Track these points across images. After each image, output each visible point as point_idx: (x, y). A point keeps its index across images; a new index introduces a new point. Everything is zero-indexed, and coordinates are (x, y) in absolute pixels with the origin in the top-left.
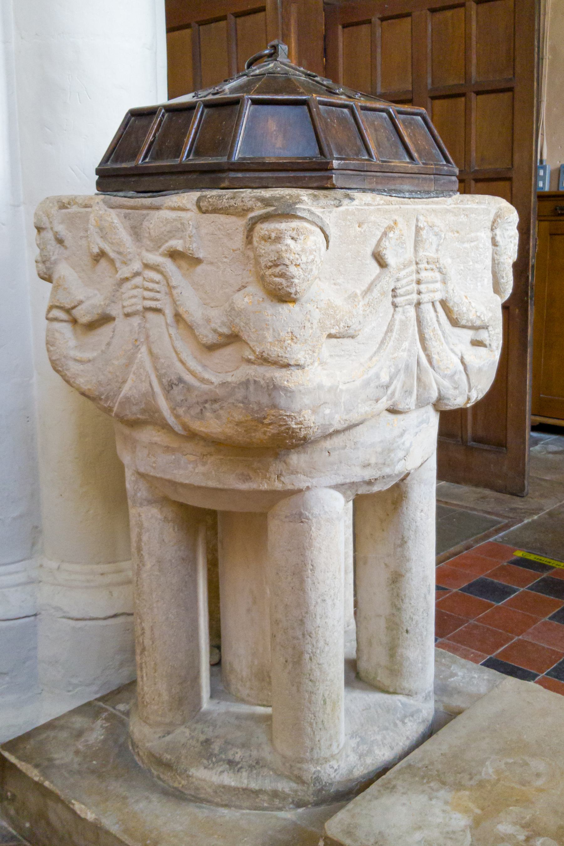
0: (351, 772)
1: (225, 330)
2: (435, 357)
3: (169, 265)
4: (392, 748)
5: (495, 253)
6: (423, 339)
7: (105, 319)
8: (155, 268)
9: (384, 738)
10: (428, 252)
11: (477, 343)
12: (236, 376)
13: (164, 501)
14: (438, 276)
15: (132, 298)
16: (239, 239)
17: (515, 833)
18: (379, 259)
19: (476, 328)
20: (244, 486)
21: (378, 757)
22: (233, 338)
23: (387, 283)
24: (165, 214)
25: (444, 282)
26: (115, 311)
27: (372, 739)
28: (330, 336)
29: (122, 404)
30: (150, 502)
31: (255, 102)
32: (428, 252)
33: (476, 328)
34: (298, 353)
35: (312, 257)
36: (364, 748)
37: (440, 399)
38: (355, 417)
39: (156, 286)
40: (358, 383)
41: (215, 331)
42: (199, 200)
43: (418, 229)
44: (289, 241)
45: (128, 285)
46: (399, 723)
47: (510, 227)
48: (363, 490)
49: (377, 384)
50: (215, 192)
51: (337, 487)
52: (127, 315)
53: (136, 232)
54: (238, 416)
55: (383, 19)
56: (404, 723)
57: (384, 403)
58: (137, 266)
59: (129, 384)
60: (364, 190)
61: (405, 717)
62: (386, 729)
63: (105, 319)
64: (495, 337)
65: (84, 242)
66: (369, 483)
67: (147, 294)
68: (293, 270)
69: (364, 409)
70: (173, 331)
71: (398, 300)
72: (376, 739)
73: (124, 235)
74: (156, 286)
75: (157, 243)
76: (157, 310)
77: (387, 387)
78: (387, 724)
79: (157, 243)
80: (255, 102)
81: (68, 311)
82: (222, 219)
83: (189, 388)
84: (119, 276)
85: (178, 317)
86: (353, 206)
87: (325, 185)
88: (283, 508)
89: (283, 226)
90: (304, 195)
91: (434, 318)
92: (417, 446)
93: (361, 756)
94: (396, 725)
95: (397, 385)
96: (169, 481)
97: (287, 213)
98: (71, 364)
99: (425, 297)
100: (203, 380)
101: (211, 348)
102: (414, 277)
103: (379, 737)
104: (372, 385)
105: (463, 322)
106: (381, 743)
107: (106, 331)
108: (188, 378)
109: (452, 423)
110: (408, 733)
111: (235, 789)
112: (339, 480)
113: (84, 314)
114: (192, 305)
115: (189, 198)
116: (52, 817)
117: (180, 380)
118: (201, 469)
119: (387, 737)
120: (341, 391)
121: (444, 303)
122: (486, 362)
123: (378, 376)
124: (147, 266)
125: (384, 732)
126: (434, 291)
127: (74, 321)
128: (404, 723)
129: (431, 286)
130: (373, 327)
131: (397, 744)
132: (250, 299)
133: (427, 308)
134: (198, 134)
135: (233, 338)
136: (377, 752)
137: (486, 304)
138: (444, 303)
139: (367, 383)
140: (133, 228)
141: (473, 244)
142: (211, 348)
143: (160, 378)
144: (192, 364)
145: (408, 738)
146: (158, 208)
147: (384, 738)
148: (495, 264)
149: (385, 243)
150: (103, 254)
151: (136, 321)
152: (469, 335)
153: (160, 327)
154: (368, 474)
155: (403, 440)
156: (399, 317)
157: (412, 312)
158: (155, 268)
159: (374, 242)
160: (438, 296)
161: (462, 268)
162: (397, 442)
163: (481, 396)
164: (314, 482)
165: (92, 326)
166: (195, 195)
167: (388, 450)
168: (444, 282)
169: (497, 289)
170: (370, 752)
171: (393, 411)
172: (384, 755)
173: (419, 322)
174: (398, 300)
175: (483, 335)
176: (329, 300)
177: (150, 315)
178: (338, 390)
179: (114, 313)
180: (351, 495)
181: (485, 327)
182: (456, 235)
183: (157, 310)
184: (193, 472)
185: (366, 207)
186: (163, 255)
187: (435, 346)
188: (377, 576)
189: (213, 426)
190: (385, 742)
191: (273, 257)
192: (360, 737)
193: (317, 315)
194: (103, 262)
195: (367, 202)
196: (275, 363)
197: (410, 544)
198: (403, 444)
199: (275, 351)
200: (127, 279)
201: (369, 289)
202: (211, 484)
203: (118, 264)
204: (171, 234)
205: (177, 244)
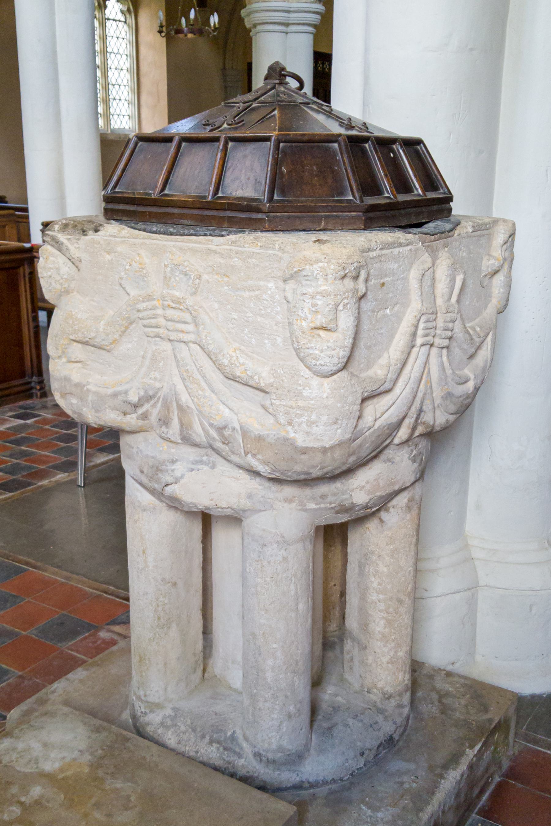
0: (148, 724)
4: (179, 743)
9: (184, 733)
17: (29, 796)
21: (166, 736)
27: (179, 724)
35: (49, 273)
36: (169, 722)
40: (110, 391)
46: (208, 738)
47: (308, 283)
49: (124, 399)
56: (211, 742)
61: (219, 742)
62: (194, 730)
72: (180, 727)
78: (199, 729)
86: (99, 236)
93: (162, 724)
94: (203, 737)
103: (183, 728)
104: (120, 398)
106: (178, 732)
110: (202, 751)
119: (187, 734)
120: (88, 390)
123: (126, 392)
125: (190, 730)
128: (211, 742)
131: (186, 746)
134: (302, 144)
136: (170, 733)
139: (115, 395)
141: (252, 293)
145: (197, 752)
147: (184, 733)
155: (173, 467)
161: (236, 317)
162: (167, 466)
170: (167, 728)
172: (169, 739)
176: (71, 311)
178: (85, 389)
182: (226, 279)
185: (112, 239)
190: (181, 734)
192: (176, 714)
195: (111, 234)
198: (173, 471)
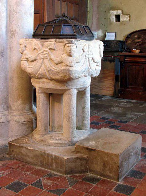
1: (60, 61)
2: (91, 67)
3: (49, 50)
5: (100, 50)
6: (89, 64)
7: (35, 60)
8: (46, 51)
10: (90, 49)
11: (97, 66)
12: (63, 68)
13: (44, 93)
14: (91, 53)
15: (41, 56)
16: (62, 47)
18: (83, 51)
19: (97, 63)
20: (60, 88)
22: (61, 62)
23: (84, 54)
24: (48, 42)
25: (93, 54)
26: (38, 59)
28: (77, 62)
29: (38, 75)
30: (41, 93)
31: (64, 25)
32: (90, 49)
33: (97, 63)
34: (72, 64)
37: (92, 75)
38: (80, 76)
39: (47, 54)
41: (58, 61)
42: (55, 40)
43: (89, 46)
44: (72, 47)
45: (41, 54)
48: (80, 90)
50: (58, 39)
51: (76, 89)
52: (40, 59)
53: (42, 45)
54: (62, 75)
55: (75, 4)
57: (84, 74)
58: (42, 51)
59: (40, 71)
60: (81, 39)
63: (35, 60)
64: (100, 64)
65: (31, 47)
66: (81, 88)
67: (44, 55)
68: (72, 51)
69: (81, 75)
70: (49, 62)
71: (86, 57)
73: (40, 46)
74: (47, 54)
75: (47, 47)
76: (47, 58)
77: (84, 71)
79: (47, 47)
80: (64, 25)
81: (27, 59)
82: (59, 43)
83: (53, 71)
84: (39, 52)
85: (50, 59)
87: (75, 38)
88: (67, 92)
89: (71, 45)
90: (73, 40)
91: (91, 60)
92: (87, 82)
95: (86, 71)
96: (46, 88)
97: (71, 43)
98: (27, 68)
99: (90, 57)
100: (55, 70)
101: (57, 64)
102: (88, 53)
105: (95, 62)
107: (35, 62)
108: (53, 69)
109: (93, 79)
111: (58, 143)
112: (76, 87)
113: (30, 59)
114: (53, 57)
115: (53, 40)
116: (22, 152)
117: (51, 70)
118: (53, 85)
121: (92, 58)
122: (99, 68)
124: (44, 51)
126: (91, 56)
127: (28, 61)
129: (91, 55)
130: (82, 62)
132: (65, 56)
133: (90, 59)
135: (61, 62)
137: (99, 59)
138: (92, 58)
139: (81, 70)
140: (42, 44)
142: (57, 64)
143: (47, 70)
144: (53, 67)
146: (47, 41)
148: (100, 52)
149: (84, 48)
150: (35, 49)
151: (42, 60)
152: (96, 64)
153: (47, 61)
154: (81, 87)
156: (86, 60)
157: (88, 59)
158: (46, 51)
159: (82, 47)
160: (92, 57)
163: (98, 75)
164: (72, 87)
165: (32, 61)
166: (55, 39)
167: (84, 82)
168: (93, 54)
169: (100, 57)
171: (85, 76)
173: (89, 61)
174: (86, 57)
175: (98, 64)
177: (45, 59)
179: (37, 59)
180: (78, 90)
181: (99, 63)
183: (47, 58)
184: (51, 86)
186: (48, 49)
187: (91, 65)
188: (81, 108)
189: (57, 77)
191: (69, 49)
193: (75, 59)
194: (35, 50)
196: (69, 66)
197: (86, 102)
199: (68, 64)
200: (40, 53)
201: (82, 55)
202: (55, 88)
203: (38, 51)
204: (50, 46)
205: (51, 47)
